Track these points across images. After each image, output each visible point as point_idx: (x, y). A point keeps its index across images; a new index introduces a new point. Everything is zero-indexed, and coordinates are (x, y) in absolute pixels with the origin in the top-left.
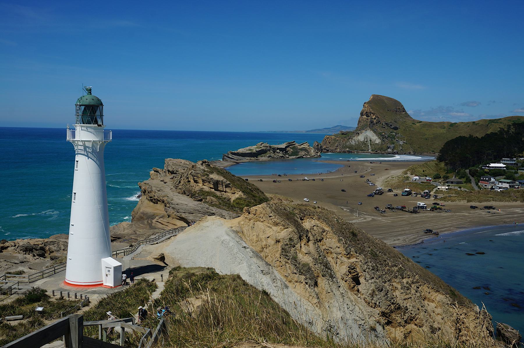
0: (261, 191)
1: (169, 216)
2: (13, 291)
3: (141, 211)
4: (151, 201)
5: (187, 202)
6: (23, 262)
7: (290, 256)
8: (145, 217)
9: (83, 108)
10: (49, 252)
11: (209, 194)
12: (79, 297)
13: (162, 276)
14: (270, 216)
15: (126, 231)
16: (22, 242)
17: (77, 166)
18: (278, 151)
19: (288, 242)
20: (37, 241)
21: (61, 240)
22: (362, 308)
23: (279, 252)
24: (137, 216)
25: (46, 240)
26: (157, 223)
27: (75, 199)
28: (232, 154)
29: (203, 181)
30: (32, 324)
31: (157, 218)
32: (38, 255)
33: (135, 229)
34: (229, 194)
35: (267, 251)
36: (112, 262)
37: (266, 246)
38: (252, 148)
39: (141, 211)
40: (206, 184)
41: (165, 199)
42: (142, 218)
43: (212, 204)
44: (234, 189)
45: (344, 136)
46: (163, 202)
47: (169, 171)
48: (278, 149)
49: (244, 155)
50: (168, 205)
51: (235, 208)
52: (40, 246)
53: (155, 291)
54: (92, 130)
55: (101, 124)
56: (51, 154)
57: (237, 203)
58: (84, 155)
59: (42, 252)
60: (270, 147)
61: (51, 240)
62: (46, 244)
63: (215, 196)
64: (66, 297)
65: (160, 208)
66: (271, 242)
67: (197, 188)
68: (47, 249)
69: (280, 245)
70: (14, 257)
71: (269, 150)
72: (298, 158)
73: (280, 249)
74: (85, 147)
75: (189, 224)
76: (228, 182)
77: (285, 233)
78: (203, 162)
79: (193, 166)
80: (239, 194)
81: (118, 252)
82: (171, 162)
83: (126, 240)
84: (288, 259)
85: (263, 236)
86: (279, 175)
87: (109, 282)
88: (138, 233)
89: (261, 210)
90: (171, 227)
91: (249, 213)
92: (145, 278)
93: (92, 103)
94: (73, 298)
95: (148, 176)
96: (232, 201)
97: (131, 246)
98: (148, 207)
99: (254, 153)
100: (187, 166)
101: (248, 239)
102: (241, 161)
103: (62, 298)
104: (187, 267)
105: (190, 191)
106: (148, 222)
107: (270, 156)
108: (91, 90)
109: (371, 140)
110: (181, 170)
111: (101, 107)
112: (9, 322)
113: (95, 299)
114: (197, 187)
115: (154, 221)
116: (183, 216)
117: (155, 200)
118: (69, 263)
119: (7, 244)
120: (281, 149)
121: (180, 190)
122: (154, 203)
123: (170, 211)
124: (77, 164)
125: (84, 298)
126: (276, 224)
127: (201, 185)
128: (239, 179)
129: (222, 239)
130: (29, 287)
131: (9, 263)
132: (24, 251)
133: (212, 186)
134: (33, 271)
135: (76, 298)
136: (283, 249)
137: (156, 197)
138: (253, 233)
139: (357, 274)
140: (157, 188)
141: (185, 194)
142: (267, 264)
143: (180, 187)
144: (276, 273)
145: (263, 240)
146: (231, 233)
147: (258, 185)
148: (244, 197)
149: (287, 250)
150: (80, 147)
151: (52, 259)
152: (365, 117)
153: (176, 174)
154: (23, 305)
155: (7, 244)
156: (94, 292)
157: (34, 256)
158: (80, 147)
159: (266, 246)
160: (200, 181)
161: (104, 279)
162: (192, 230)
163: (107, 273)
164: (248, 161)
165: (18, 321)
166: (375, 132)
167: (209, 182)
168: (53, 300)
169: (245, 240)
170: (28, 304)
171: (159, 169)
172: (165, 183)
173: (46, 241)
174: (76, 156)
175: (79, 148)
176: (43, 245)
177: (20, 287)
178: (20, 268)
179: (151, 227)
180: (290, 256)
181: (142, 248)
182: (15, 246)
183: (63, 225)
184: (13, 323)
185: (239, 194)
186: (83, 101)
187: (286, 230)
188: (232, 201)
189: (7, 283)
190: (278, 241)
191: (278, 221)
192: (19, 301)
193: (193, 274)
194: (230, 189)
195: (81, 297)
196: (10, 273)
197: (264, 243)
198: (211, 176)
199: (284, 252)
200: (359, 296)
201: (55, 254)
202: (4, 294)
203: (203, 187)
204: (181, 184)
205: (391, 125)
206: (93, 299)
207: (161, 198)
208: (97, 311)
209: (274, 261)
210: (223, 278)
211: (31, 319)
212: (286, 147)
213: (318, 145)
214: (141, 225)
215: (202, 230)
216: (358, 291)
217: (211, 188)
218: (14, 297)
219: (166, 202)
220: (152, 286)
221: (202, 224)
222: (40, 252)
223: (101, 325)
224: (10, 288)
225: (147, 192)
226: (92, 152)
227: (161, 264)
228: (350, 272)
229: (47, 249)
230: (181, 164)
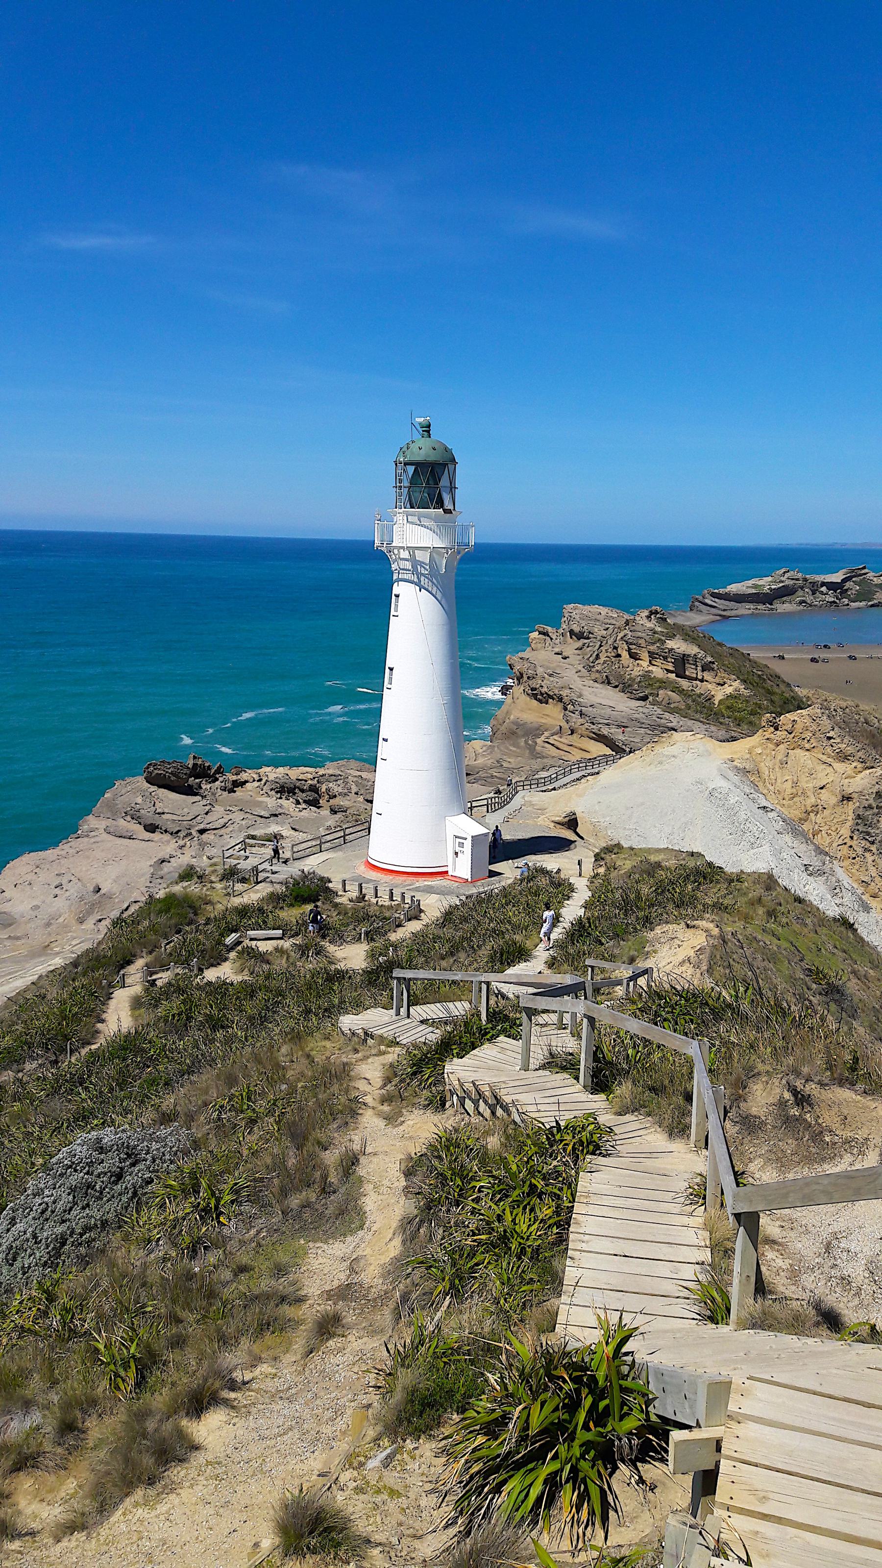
0: (784, 682)
1: (572, 732)
2: (262, 876)
4: (535, 696)
5: (622, 705)
7: (877, 835)
8: (519, 732)
9: (411, 469)
11: (663, 684)
12: (397, 897)
13: (579, 863)
14: (829, 738)
15: (480, 761)
16: (272, 773)
17: (396, 606)
18: (824, 589)
19: (871, 801)
21: (351, 772)
23: (849, 824)
24: (503, 728)
25: (321, 771)
26: (547, 745)
28: (714, 595)
29: (651, 655)
30: (303, 950)
31: (546, 734)
32: (305, 802)
33: (499, 756)
34: (710, 686)
35: (819, 819)
36: (471, 828)
37: (816, 809)
38: (761, 583)
39: (512, 717)
40: (658, 662)
41: (564, 693)
43: (669, 708)
46: (560, 700)
47: (572, 632)
48: (823, 584)
49: (739, 598)
50: (570, 707)
52: (310, 782)
53: (569, 898)
54: (431, 524)
55: (451, 507)
56: (358, 582)
57: (728, 707)
58: (412, 582)
60: (805, 580)
61: (331, 772)
62: (321, 779)
65: (552, 714)
66: (829, 798)
67: (637, 672)
68: (323, 790)
69: (851, 807)
70: (259, 804)
71: (802, 588)
72: (872, 606)
73: (851, 816)
74: (415, 563)
75: (619, 750)
76: (709, 659)
78: (651, 613)
79: (627, 623)
80: (733, 686)
81: (474, 804)
82: (578, 613)
83: (481, 779)
84: (873, 843)
85: (808, 784)
86: (825, 646)
87: (463, 868)
88: (505, 764)
89: (808, 721)
90: (577, 755)
91: (776, 729)
93: (433, 457)
94: (385, 900)
95: (527, 643)
96: (716, 702)
97: (498, 792)
98: (523, 709)
100: (614, 622)
101: (772, 788)
102: (733, 613)
103: (362, 898)
106: (526, 742)
107: (804, 602)
108: (429, 426)
110: (599, 631)
111: (451, 467)
112: (254, 943)
113: (433, 907)
114: (637, 669)
115: (539, 741)
116: (606, 733)
117: (542, 694)
118: (376, 823)
119: (244, 776)
120: (831, 586)
121: (597, 675)
122: (541, 701)
125: (408, 900)
126: (844, 757)
127: (645, 664)
128: (734, 653)
129: (711, 786)
131: (248, 815)
134: (301, 836)
135: (391, 899)
136: (859, 817)
137: (545, 690)
138: (783, 775)
140: (548, 668)
141: (609, 683)
142: (819, 851)
143: (599, 668)
144: (840, 873)
145: (809, 793)
146: (731, 774)
147: (777, 667)
148: (746, 692)
150: (403, 564)
151: (334, 812)
153: (588, 638)
154: (282, 908)
155: (244, 776)
156: (430, 890)
157: (298, 803)
159: (816, 809)
160: (645, 655)
161: (450, 863)
162: (636, 763)
164: (750, 612)
165: (274, 943)
167: (665, 658)
168: (343, 900)
169: (765, 792)
170: (292, 905)
171: (549, 629)
173: (320, 773)
175: (400, 564)
176: (315, 782)
177: (275, 868)
179: (535, 755)
180: (877, 835)
181: (523, 797)
182: (260, 780)
183: (361, 739)
184: (265, 947)
185: (733, 686)
186: (412, 453)
187: (868, 771)
188: (716, 702)
189: (247, 857)
190: (847, 798)
191: (850, 750)
192: (275, 899)
193: (658, 865)
194: (713, 673)
195: (403, 897)
197: (812, 800)
198: (670, 644)
202: (244, 880)
203: (651, 668)
204: (601, 661)
207: (557, 692)
208: (440, 932)
209: (835, 845)
210: (738, 880)
211: (298, 940)
212: (844, 581)
214: (511, 748)
215: (660, 763)
217: (668, 671)
218: (262, 891)
219: (565, 699)
220: (562, 889)
221: (658, 748)
222: (311, 796)
223: (488, 984)
224: (255, 870)
225: (525, 678)
226: (425, 576)
227: (569, 835)
229: (323, 790)
230: (598, 617)
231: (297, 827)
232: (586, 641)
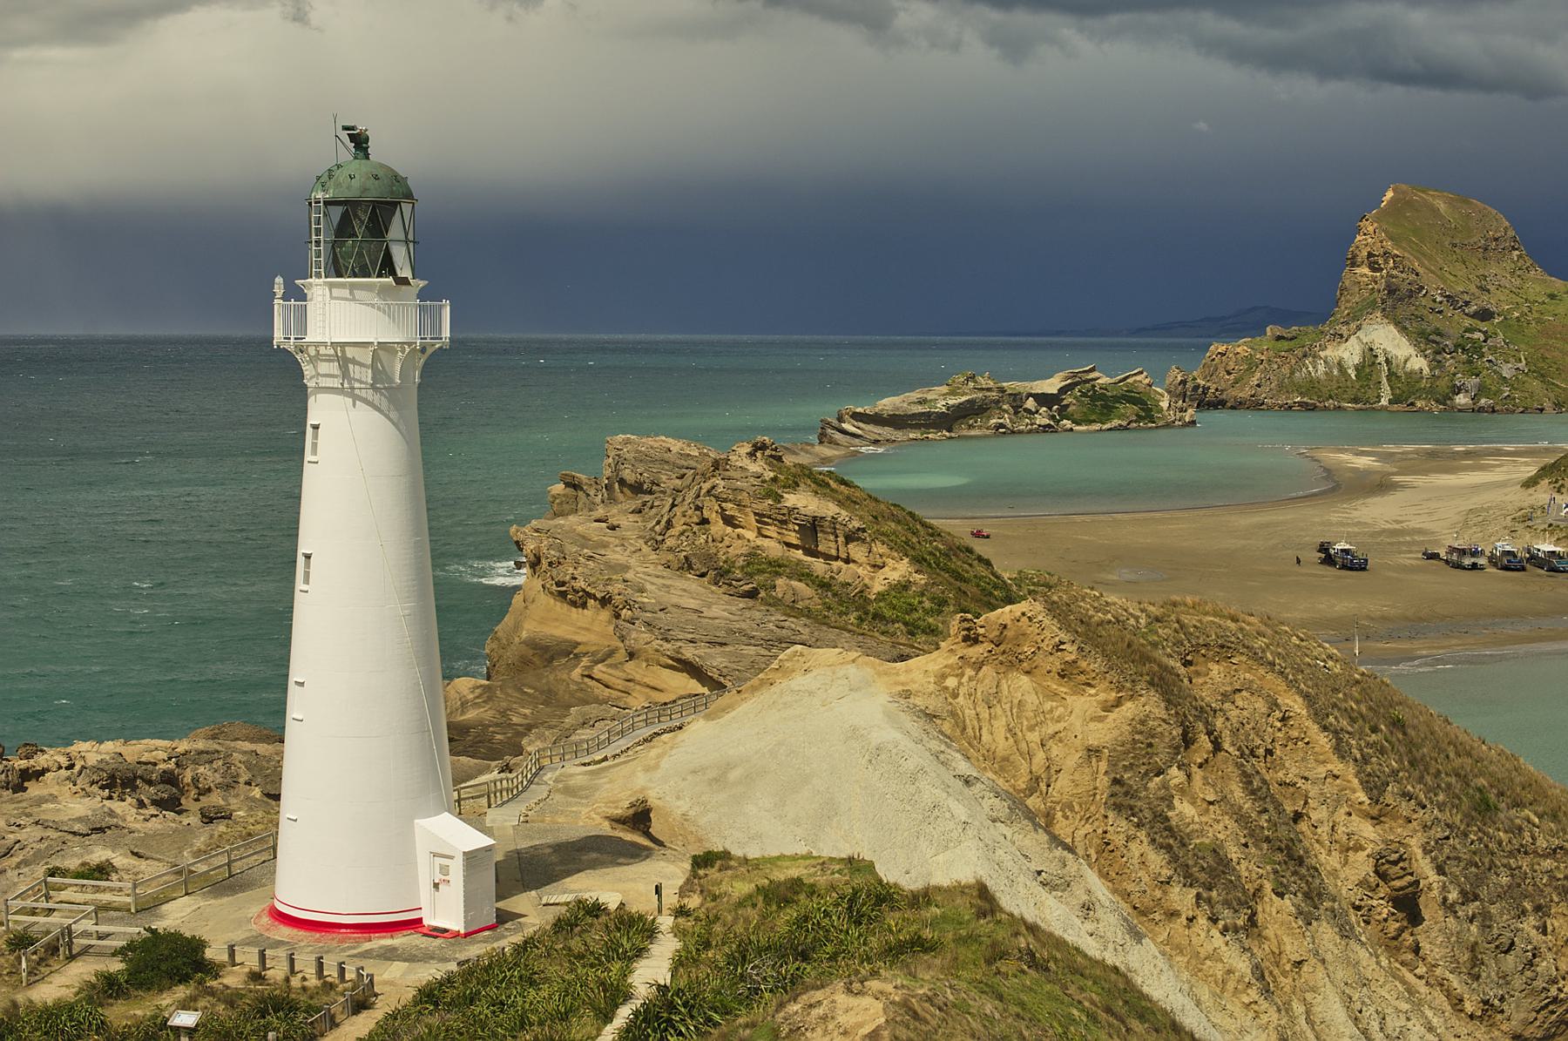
2: (79, 943)
3: (524, 635)
4: (563, 595)
6: (101, 830)
9: (336, 212)
10: (193, 793)
11: (777, 567)
13: (658, 890)
16: (92, 752)
17: (315, 446)
20: (151, 750)
22: (1435, 1021)
27: (307, 581)
28: (857, 416)
29: (760, 517)
31: (585, 661)
32: (155, 803)
42: (525, 662)
44: (879, 548)
45: (1285, 344)
47: (622, 482)
50: (625, 613)
51: (891, 626)
52: (162, 766)
53: (640, 953)
59: (169, 791)
60: (1002, 390)
62: (181, 760)
63: (805, 575)
64: (277, 972)
67: (738, 549)
68: (188, 779)
75: (718, 686)
76: (856, 524)
77: (1090, 719)
80: (899, 569)
87: (447, 911)
92: (590, 896)
105: (710, 558)
109: (1387, 361)
119: (41, 761)
120: (1044, 399)
121: (671, 557)
122: (574, 604)
132: (102, 788)
133: (793, 538)
136: (1116, 782)
139: (1411, 884)
141: (690, 567)
143: (670, 542)
149: (1130, 789)
153: (651, 492)
155: (41, 761)
156: (389, 955)
157: (141, 804)
158: (324, 367)
166: (1403, 330)
172: (613, 528)
173: (181, 749)
174: (311, 401)
176: (171, 765)
177: (103, 928)
185: (899, 569)
186: (338, 185)
189: (51, 911)
190: (1093, 752)
196: (63, 873)
198: (791, 500)
199: (1123, 799)
200: (1421, 970)
203: (760, 541)
205: (1467, 303)
206: (391, 983)
212: (1063, 390)
213: (1184, 382)
216: (1416, 950)
217: (789, 545)
219: (617, 599)
222: (165, 792)
229: (188, 779)
230: (667, 456)
232: (647, 498)
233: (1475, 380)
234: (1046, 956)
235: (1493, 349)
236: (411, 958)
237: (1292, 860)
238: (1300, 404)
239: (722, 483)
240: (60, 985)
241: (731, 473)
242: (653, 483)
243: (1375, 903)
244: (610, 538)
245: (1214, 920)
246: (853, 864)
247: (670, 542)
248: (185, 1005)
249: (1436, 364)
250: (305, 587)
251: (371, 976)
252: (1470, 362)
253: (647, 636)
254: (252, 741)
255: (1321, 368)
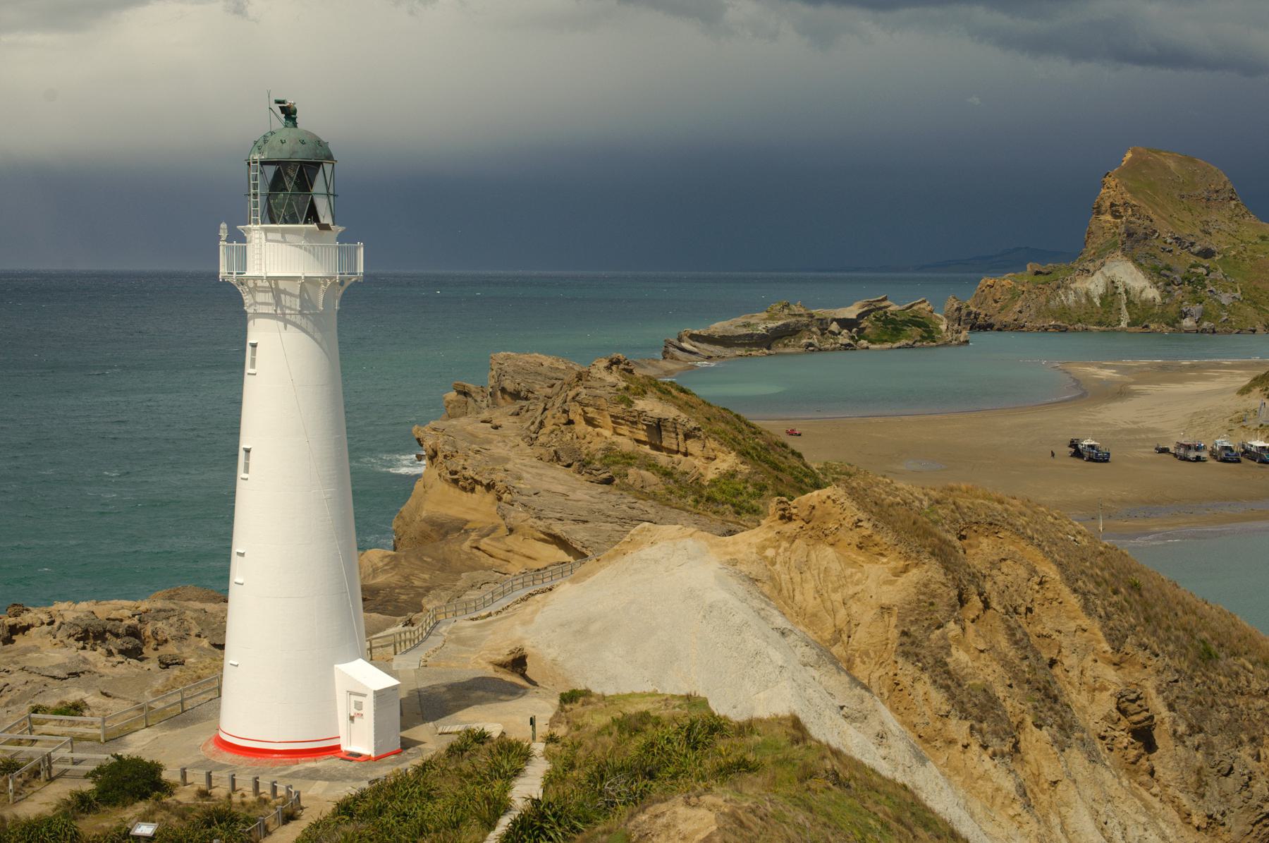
3: (424, 514)
4: (456, 482)
6: (76, 674)
9: (270, 171)
10: (153, 644)
11: (628, 459)
13: (532, 722)
16: (71, 611)
17: (253, 361)
20: (119, 609)
29: (615, 419)
31: (473, 536)
32: (121, 652)
33: (407, 571)
38: (752, 321)
41: (497, 477)
43: (642, 493)
44: (712, 444)
47: (503, 390)
50: (506, 497)
51: (722, 506)
52: (127, 622)
53: (517, 772)
59: (133, 644)
60: (811, 316)
62: (142, 617)
63: (651, 466)
64: (221, 790)
67: (597, 445)
76: (693, 424)
93: (302, 154)
99: (762, 336)
100: (561, 376)
104: (610, 691)
105: (574, 451)
109: (1126, 292)
110: (541, 389)
119: (26, 618)
120: (845, 324)
121: (543, 451)
122: (464, 489)
123: (517, 515)
124: (254, 353)
125: (281, 792)
130: (103, 757)
132: (78, 640)
133: (642, 436)
136: (904, 633)
139: (1147, 719)
149: (916, 641)
152: (1108, 217)
153: (526, 399)
156: (313, 775)
157: (110, 653)
158: (261, 297)
163: (353, 712)
166: (1140, 266)
172: (496, 428)
174: (250, 324)
176: (135, 621)
177: (77, 756)
178: (74, 694)
185: (727, 461)
189: (34, 741)
198: (640, 404)
199: (910, 647)
200: (1156, 790)
201: (171, 649)
203: (616, 439)
205: (1192, 244)
212: (861, 316)
213: (959, 309)
217: (638, 441)
219: (499, 486)
222: (130, 643)
225: (440, 455)
228: (1124, 712)
229: (148, 632)
230: (540, 369)
231: (109, 692)
232: (524, 403)
233: (1198, 307)
234: (846, 776)
235: (1214, 282)
236: (331, 777)
237: (1048, 698)
238: (1054, 327)
239: (584, 391)
240: (41, 803)
241: (592, 383)
242: (529, 391)
243: (1117, 734)
244: (494, 435)
245: (985, 747)
246: (690, 700)
247: (542, 439)
248: (145, 819)
249: (1167, 293)
250: (245, 476)
251: (298, 794)
252: (1194, 292)
253: (524, 515)
254: (202, 601)
255: (1072, 297)
